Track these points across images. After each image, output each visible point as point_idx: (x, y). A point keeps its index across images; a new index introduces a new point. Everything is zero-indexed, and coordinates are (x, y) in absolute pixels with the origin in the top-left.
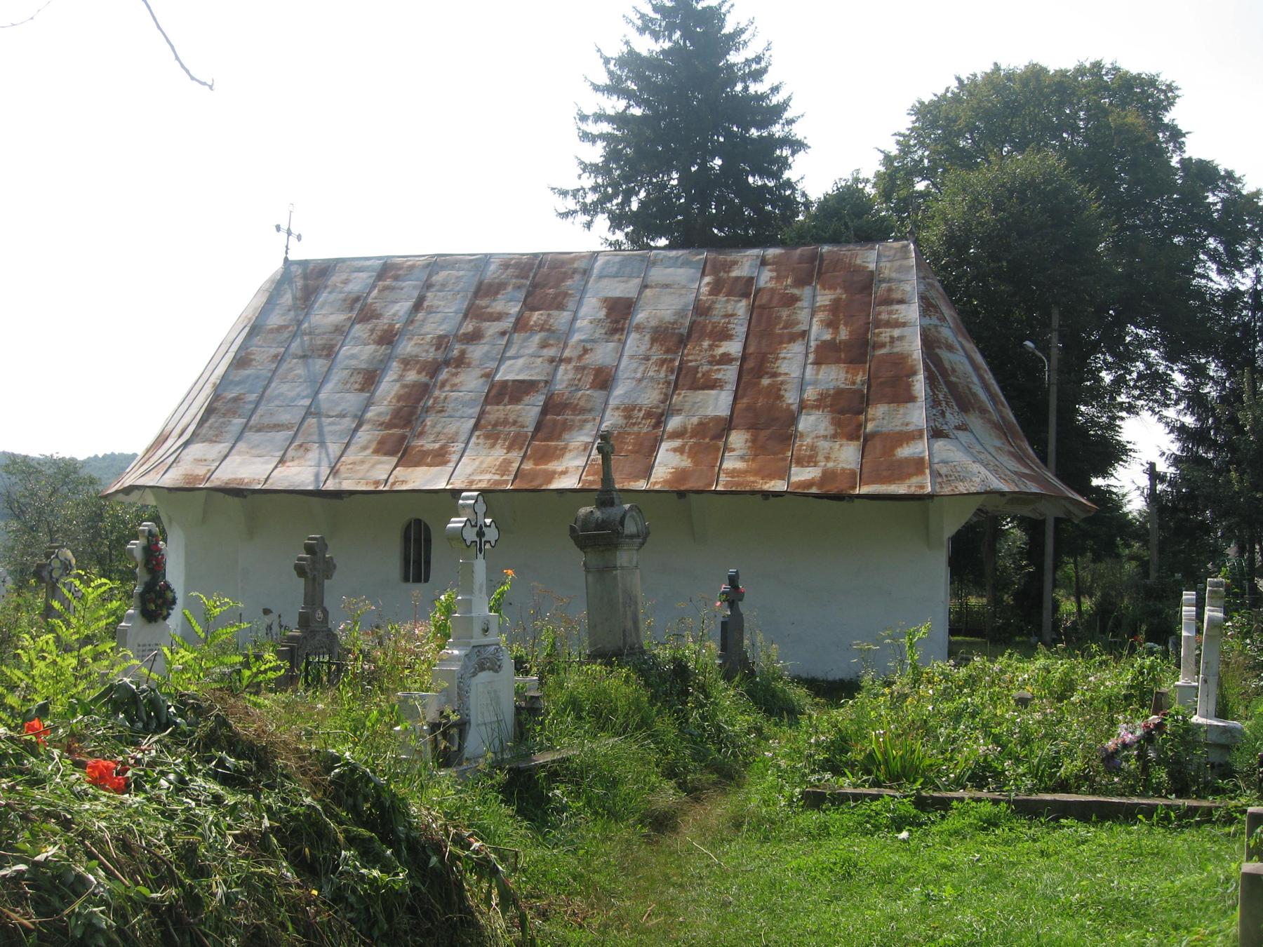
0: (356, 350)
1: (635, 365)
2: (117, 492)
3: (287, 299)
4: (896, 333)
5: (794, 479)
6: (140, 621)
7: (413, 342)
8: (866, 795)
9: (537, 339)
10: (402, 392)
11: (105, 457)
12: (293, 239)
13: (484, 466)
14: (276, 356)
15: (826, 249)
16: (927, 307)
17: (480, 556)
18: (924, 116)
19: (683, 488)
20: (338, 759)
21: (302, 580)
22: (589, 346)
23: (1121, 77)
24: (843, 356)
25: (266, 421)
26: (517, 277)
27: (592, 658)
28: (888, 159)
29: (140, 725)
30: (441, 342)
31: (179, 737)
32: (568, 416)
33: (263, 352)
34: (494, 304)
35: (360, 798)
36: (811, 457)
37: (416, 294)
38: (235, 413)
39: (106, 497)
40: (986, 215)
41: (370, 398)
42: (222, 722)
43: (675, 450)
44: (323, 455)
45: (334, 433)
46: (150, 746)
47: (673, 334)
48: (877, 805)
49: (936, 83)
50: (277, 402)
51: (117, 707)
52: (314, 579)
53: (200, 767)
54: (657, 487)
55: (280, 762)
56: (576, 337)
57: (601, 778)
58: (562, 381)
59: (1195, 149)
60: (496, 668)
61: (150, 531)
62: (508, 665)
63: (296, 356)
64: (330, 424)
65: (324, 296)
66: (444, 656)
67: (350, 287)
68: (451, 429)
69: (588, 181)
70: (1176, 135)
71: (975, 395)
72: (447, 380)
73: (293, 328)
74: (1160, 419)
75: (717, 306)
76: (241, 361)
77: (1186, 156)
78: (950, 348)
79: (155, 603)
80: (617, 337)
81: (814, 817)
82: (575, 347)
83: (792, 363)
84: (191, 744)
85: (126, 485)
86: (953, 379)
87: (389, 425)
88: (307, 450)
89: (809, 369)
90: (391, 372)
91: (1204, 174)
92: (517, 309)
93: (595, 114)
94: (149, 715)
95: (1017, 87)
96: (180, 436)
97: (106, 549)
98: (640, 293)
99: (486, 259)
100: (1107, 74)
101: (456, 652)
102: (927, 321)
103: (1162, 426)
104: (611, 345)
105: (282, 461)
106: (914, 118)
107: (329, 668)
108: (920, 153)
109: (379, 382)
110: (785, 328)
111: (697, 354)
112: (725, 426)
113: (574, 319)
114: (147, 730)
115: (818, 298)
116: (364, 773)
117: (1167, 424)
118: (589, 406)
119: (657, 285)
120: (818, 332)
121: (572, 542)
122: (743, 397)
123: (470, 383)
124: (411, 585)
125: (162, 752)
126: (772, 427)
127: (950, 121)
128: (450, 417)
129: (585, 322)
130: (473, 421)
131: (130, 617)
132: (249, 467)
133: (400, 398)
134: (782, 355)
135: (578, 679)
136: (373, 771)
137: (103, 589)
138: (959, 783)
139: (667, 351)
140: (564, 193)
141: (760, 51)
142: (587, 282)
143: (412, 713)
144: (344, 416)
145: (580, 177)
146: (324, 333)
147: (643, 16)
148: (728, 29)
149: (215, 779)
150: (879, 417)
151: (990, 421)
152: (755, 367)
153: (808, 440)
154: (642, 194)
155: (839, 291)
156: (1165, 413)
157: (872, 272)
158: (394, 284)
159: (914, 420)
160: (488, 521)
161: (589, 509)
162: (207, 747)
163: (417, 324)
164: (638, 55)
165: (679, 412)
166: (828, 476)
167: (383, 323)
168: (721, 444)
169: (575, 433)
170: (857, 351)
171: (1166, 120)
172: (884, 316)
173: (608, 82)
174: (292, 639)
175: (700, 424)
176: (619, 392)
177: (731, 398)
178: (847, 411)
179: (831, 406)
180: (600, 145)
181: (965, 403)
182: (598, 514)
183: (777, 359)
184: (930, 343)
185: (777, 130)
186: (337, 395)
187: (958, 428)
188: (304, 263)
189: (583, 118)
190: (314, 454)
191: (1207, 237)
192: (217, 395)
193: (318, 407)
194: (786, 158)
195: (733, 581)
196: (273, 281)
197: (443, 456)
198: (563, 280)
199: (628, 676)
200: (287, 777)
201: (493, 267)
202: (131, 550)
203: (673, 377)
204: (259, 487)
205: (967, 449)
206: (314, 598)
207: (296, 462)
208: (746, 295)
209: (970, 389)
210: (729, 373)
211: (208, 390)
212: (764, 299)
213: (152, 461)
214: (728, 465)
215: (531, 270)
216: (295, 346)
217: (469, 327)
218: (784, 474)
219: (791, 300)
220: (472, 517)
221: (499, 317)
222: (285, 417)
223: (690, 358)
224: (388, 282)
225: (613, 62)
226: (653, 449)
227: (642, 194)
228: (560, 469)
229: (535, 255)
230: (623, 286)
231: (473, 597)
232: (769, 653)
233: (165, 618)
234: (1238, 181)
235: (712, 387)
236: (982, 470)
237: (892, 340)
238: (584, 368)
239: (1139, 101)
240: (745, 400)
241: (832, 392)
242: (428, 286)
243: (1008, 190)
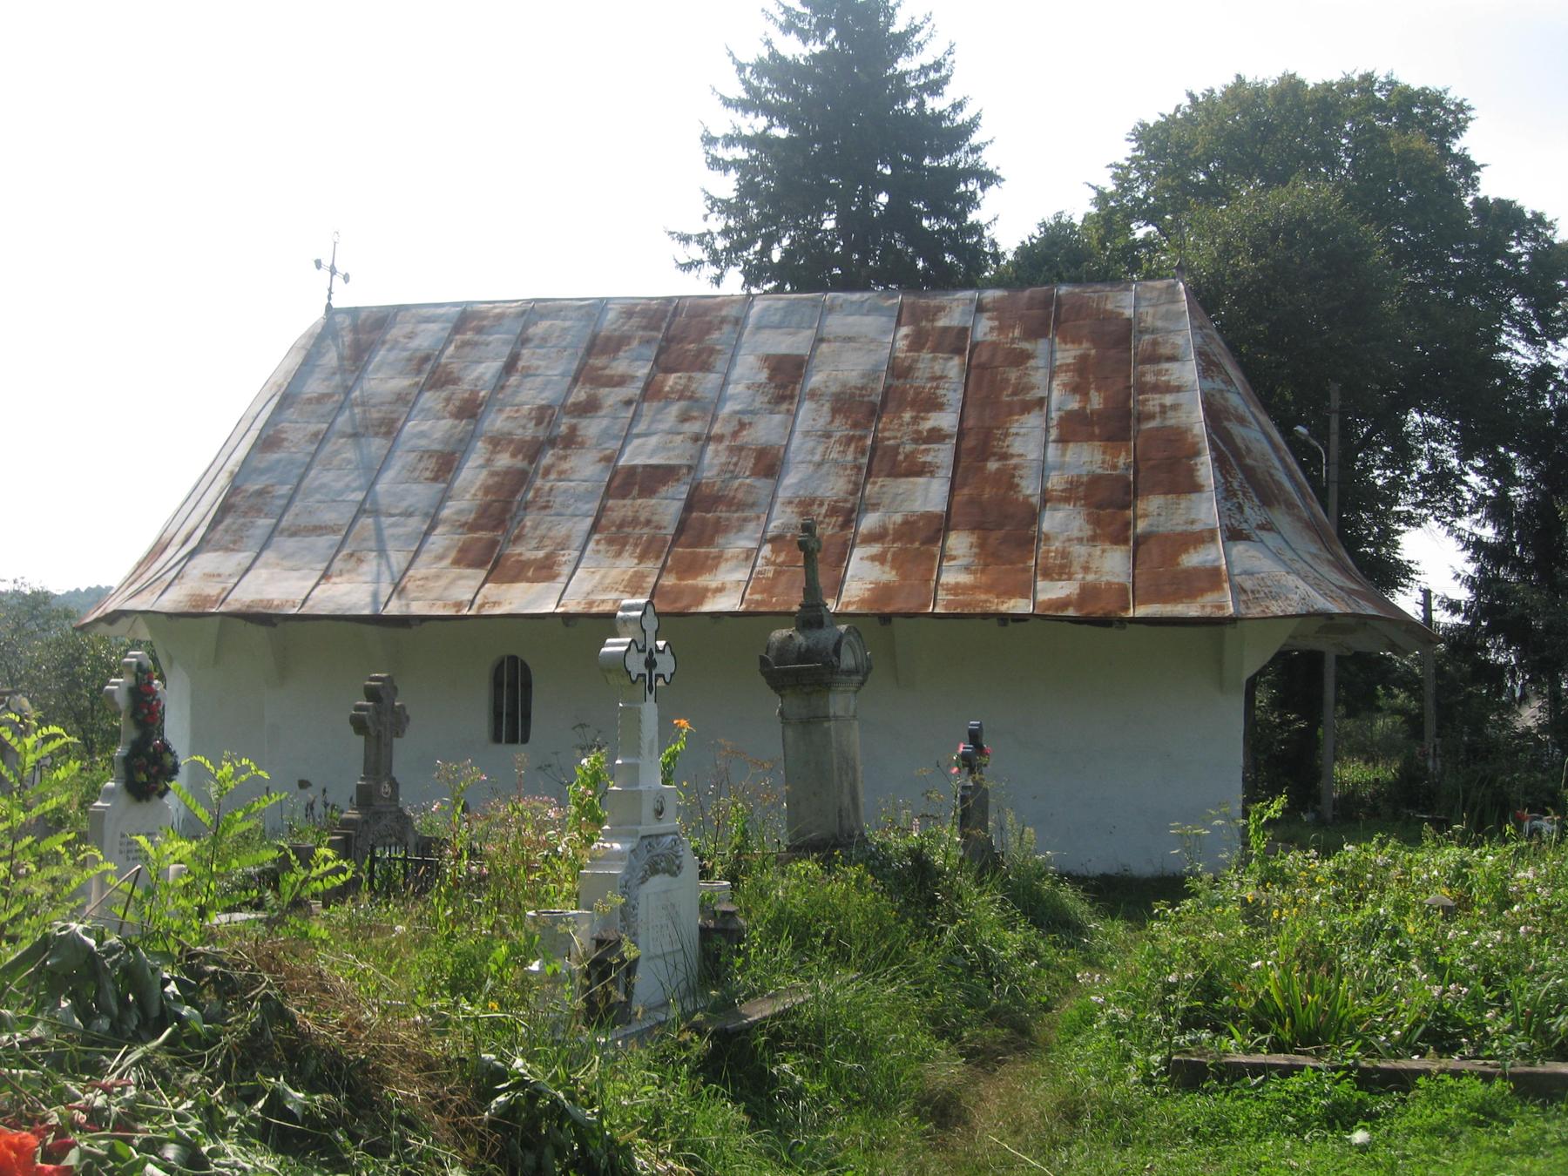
0: (426, 426)
1: (811, 444)
2: (98, 620)
3: (331, 358)
4: (1168, 399)
5: (1041, 597)
6: (124, 799)
7: (504, 415)
8: (1273, 1066)
9: (674, 410)
10: (490, 482)
11: (89, 591)
12: (338, 280)
13: (608, 581)
14: (316, 435)
15: (1063, 290)
16: (1208, 365)
17: (651, 697)
18: (1148, 144)
19: (887, 610)
20: (501, 1075)
21: (362, 739)
22: (746, 419)
23: (1400, 93)
24: (1097, 431)
25: (304, 521)
26: (644, 328)
27: (799, 849)
28: (1102, 198)
29: (104, 1023)
30: (543, 415)
31: (187, 1049)
32: (722, 513)
33: (298, 430)
34: (614, 364)
35: (549, 1151)
36: (1062, 567)
37: (507, 350)
38: (259, 511)
39: (83, 628)
40: (1243, 263)
41: (445, 491)
42: (275, 1012)
43: (873, 558)
44: (384, 568)
45: (396, 538)
46: (125, 1069)
47: (862, 403)
48: (1295, 1083)
49: (1162, 100)
50: (318, 497)
51: (56, 982)
52: (378, 737)
53: (231, 1114)
54: (851, 609)
55: (396, 1093)
56: (728, 408)
57: (849, 1042)
58: (711, 466)
59: (1491, 187)
60: (673, 869)
61: (139, 665)
62: (690, 864)
63: (343, 435)
64: (392, 525)
65: (381, 355)
66: (596, 851)
67: (414, 344)
68: (561, 531)
69: (717, 223)
70: (1468, 167)
71: (1279, 485)
72: (552, 466)
73: (339, 397)
74: (1450, 533)
75: (920, 365)
76: (268, 441)
77: (1481, 195)
78: (1242, 421)
79: (148, 772)
80: (784, 406)
81: (1195, 1107)
82: (727, 421)
83: (1027, 440)
84: (213, 1062)
85: (109, 610)
86: (1249, 461)
87: (473, 527)
88: (360, 561)
89: (1052, 448)
90: (474, 456)
91: (1506, 217)
92: (646, 371)
93: (726, 136)
94: (123, 1001)
95: (1270, 103)
96: (184, 543)
97: (87, 704)
98: (814, 349)
99: (602, 304)
100: (1380, 90)
101: (617, 846)
102: (1209, 384)
103: (1452, 539)
104: (777, 418)
105: (325, 576)
106: (1135, 145)
107: (405, 867)
108: (1144, 188)
109: (459, 468)
110: (1014, 393)
111: (897, 429)
112: (939, 527)
113: (725, 383)
114: (119, 1037)
115: (1058, 355)
116: (555, 1102)
117: (1459, 537)
118: (750, 500)
119: (836, 339)
120: (1060, 399)
121: (763, 680)
122: (963, 485)
123: (585, 469)
124: (505, 748)
125: (150, 1086)
126: (1008, 529)
127: (1184, 148)
128: (558, 514)
129: (741, 388)
130: (589, 521)
131: (110, 794)
132: (280, 584)
133: (487, 490)
134: (1012, 430)
135: (793, 885)
136: (571, 1096)
137: (52, 746)
138: (1407, 1046)
139: (855, 426)
140: (686, 239)
141: (939, 56)
142: (740, 335)
143: (557, 945)
144: (411, 515)
145: (706, 218)
146: (382, 404)
147: (787, 10)
148: (898, 26)
149: (264, 1140)
150: (1153, 512)
151: (1300, 519)
152: (977, 448)
153: (1057, 545)
154: (786, 242)
155: (1085, 345)
156: (1459, 523)
157: (1129, 320)
158: (476, 338)
159: (1202, 516)
160: (661, 644)
161: (785, 632)
162: (247, 1068)
163: (508, 391)
164: (783, 59)
165: (875, 507)
166: (1088, 593)
167: (462, 390)
168: (937, 550)
169: (731, 536)
170: (1115, 424)
171: (1455, 150)
172: (1150, 378)
173: (744, 96)
174: (347, 823)
175: (906, 523)
176: (791, 480)
177: (946, 488)
178: (1108, 505)
179: (1086, 497)
180: (733, 175)
181: (1267, 495)
182: (800, 639)
183: (1006, 435)
184: (1215, 414)
185: (962, 158)
186: (402, 486)
187: (1261, 527)
188: (353, 312)
189: (709, 140)
190: (370, 565)
191: (1511, 297)
192: (235, 487)
193: (375, 502)
194: (974, 193)
195: (975, 737)
196: (311, 336)
197: (550, 567)
198: (708, 332)
199: (859, 880)
200: (410, 1123)
201: (611, 316)
202: (112, 692)
203: (865, 460)
204: (294, 611)
205: (1277, 556)
206: (378, 764)
207: (345, 577)
208: (959, 351)
209: (1271, 475)
210: (943, 455)
211: (223, 480)
212: (984, 356)
213: (145, 577)
214: (948, 578)
215: (663, 319)
216: (342, 421)
217: (580, 394)
218: (1027, 590)
219: (1021, 358)
220: (639, 637)
221: (621, 381)
222: (329, 517)
223: (887, 434)
224: (469, 336)
225: (749, 69)
226: (843, 557)
227: (786, 242)
228: (714, 585)
229: (669, 300)
230: (789, 340)
231: (649, 760)
232: (1025, 841)
233: (162, 795)
234: (1549, 226)
235: (920, 474)
236: (1300, 583)
237: (1164, 409)
238: (741, 448)
239: (1421, 124)
240: (966, 491)
241: (1085, 479)
242: (523, 340)
243: (1270, 230)
